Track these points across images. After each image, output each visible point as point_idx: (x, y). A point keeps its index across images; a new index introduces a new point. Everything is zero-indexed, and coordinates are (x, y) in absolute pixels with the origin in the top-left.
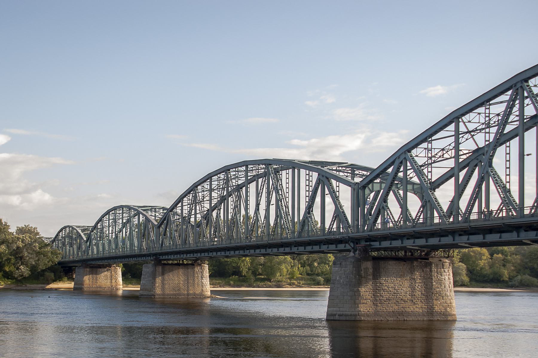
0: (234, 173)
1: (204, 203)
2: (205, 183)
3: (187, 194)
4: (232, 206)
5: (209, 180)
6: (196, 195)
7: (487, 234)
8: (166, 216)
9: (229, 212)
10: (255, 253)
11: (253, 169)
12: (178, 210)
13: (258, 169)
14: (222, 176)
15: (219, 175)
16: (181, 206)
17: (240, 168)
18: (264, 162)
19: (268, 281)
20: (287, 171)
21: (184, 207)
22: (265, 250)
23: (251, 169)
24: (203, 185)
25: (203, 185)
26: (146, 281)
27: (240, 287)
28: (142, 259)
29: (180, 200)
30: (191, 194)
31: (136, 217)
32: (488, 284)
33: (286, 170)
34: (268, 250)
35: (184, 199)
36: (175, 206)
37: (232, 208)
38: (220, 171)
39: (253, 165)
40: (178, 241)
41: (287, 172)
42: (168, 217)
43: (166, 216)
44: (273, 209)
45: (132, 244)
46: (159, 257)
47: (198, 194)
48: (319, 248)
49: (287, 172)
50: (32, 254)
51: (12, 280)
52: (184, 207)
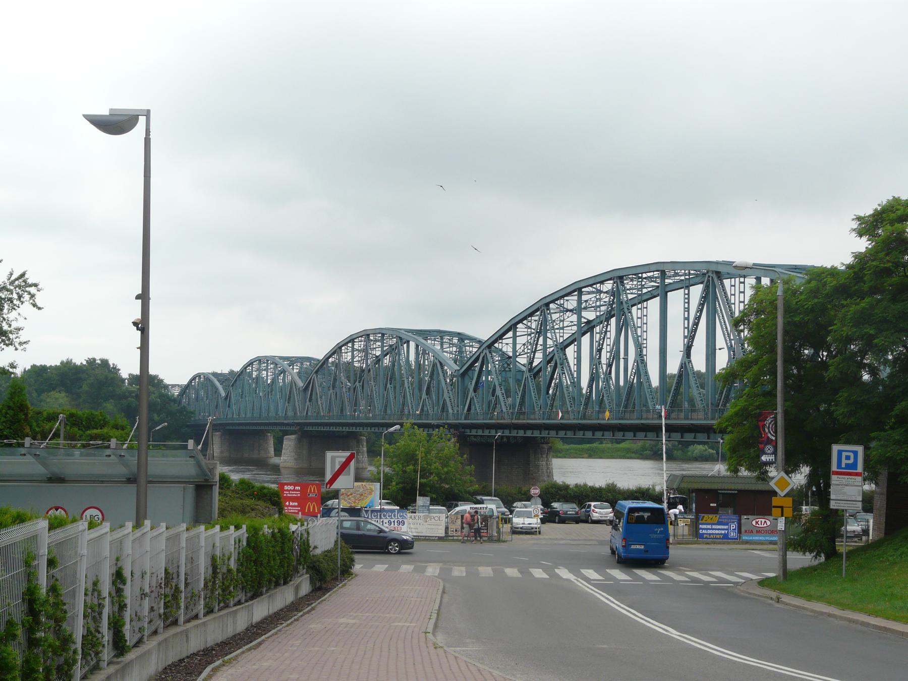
3: (527, 316)
5: (576, 293)
6: (545, 319)
7: (597, 431)
8: (311, 378)
9: (621, 357)
10: (557, 436)
16: (512, 336)
19: (874, 518)
20: (733, 280)
21: (517, 338)
22: (706, 435)
26: (287, 457)
27: (53, 434)
28: (373, 430)
29: (512, 326)
30: (537, 316)
31: (386, 358)
32: (561, 483)
33: (731, 278)
34: (543, 432)
35: (517, 326)
40: (411, 404)
41: (733, 284)
43: (311, 378)
45: (268, 411)
46: (463, 430)
47: (549, 316)
48: (633, 436)
49: (733, 284)
50: (508, 393)
52: (517, 338)
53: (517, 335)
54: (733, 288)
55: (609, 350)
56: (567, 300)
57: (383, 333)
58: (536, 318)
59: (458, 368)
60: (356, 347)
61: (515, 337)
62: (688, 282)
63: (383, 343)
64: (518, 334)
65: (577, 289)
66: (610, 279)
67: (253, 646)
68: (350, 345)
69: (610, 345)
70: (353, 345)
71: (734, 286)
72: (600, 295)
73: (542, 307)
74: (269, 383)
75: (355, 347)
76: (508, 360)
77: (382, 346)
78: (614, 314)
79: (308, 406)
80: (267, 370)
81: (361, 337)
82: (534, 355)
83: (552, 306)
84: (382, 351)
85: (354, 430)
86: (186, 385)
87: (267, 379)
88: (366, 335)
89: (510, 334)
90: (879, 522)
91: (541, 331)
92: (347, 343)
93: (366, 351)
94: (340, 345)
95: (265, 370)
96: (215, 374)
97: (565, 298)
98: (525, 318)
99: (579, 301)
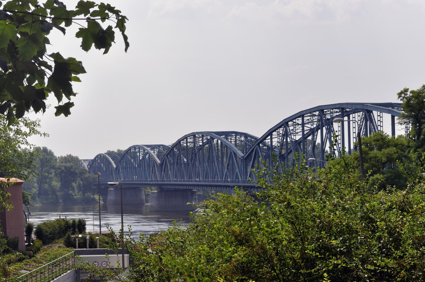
0: (309, 118)
1: (295, 136)
2: (280, 129)
4: (354, 134)
6: (286, 130)
8: (254, 149)
11: (327, 113)
12: (268, 141)
13: (332, 113)
14: (281, 131)
15: (294, 121)
17: (314, 113)
18: (337, 106)
20: (354, 114)
23: (307, 121)
24: (278, 130)
25: (278, 130)
35: (273, 133)
36: (265, 137)
37: (354, 137)
38: (295, 117)
39: (327, 109)
42: (256, 149)
43: (254, 149)
44: (151, 170)
51: (66, 222)
53: (270, 140)
54: (354, 129)
55: (359, 119)
56: (298, 120)
57: (203, 134)
58: (282, 129)
59: (243, 155)
60: (189, 140)
61: (271, 139)
62: (354, 111)
63: (203, 138)
64: (273, 137)
65: (301, 115)
66: (317, 111)
67: (159, 160)
68: (185, 140)
69: (360, 116)
70: (187, 140)
71: (355, 128)
72: (313, 118)
73: (285, 124)
74: (141, 159)
75: (188, 141)
76: (271, 148)
77: (203, 140)
78: (302, 141)
79: (163, 174)
80: (139, 152)
81: (192, 136)
82: (282, 147)
83: (290, 123)
84: (203, 142)
85: (189, 188)
86: (92, 160)
87: (140, 157)
88: (194, 135)
89: (269, 137)
90: (65, 268)
91: (286, 134)
92: (184, 139)
93: (194, 142)
94: (180, 140)
95: (138, 152)
96: (110, 153)
97: (298, 119)
98: (277, 129)
99: (303, 120)
